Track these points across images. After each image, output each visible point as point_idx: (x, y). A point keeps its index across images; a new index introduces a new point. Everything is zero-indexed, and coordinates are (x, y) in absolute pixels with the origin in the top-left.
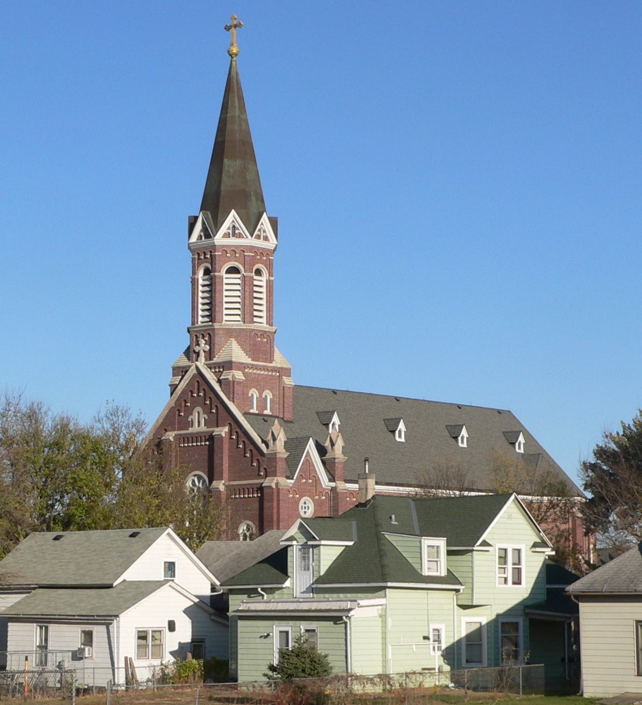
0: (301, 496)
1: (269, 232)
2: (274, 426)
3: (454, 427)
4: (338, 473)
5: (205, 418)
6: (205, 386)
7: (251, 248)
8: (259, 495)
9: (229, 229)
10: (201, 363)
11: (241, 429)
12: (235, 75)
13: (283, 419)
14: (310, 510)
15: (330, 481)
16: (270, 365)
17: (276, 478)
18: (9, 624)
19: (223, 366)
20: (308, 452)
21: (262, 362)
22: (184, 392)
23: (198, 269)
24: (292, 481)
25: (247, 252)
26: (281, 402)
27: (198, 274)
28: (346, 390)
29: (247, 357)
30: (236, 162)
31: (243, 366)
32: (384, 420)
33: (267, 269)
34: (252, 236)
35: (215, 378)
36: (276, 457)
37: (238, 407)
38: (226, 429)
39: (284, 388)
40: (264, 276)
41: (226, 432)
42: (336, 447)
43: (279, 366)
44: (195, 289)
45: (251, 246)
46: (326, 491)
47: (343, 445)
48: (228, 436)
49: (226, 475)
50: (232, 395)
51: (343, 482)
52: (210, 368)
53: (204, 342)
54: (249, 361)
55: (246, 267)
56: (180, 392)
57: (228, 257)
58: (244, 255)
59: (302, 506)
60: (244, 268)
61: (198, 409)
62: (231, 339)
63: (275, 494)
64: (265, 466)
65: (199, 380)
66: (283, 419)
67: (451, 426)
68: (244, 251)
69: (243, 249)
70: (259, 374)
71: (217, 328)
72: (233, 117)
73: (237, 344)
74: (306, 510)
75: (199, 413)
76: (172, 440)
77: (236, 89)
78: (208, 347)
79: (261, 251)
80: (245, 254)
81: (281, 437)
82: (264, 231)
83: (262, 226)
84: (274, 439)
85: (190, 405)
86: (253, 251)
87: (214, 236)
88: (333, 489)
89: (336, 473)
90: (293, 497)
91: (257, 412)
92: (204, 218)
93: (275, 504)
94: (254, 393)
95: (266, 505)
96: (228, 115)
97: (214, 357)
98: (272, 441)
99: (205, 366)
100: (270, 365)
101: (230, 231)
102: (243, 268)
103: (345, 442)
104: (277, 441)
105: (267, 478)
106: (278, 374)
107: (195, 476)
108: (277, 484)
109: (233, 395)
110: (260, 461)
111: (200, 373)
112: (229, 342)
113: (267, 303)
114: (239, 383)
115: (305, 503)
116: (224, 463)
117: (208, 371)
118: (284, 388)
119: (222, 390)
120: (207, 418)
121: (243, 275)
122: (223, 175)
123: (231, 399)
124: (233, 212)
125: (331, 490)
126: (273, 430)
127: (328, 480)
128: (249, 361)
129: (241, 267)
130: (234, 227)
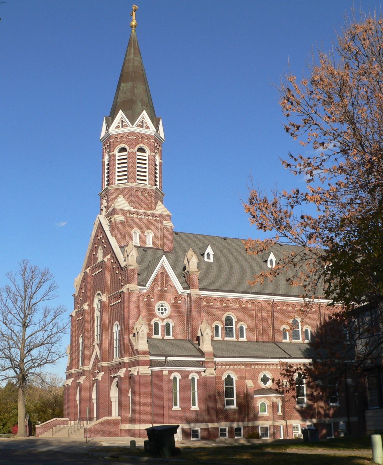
0: (156, 301)
7: (133, 133)
9: (119, 123)
12: (133, 36)
13: (163, 250)
14: (167, 312)
15: (184, 288)
16: (152, 212)
18: (130, 445)
20: (162, 266)
21: (144, 210)
25: (131, 136)
28: (237, 238)
29: (130, 206)
31: (125, 212)
33: (149, 148)
34: (133, 124)
37: (118, 240)
43: (159, 213)
45: (133, 132)
47: (197, 262)
51: (198, 290)
54: (131, 209)
57: (119, 142)
69: (128, 135)
72: (129, 60)
73: (124, 198)
74: (161, 308)
82: (146, 123)
83: (143, 120)
88: (189, 295)
89: (191, 282)
90: (149, 301)
91: (139, 245)
100: (152, 212)
106: (158, 219)
108: (128, 289)
122: (120, 93)
124: (121, 112)
127: (182, 288)
128: (131, 209)
129: (127, 147)
130: (123, 122)
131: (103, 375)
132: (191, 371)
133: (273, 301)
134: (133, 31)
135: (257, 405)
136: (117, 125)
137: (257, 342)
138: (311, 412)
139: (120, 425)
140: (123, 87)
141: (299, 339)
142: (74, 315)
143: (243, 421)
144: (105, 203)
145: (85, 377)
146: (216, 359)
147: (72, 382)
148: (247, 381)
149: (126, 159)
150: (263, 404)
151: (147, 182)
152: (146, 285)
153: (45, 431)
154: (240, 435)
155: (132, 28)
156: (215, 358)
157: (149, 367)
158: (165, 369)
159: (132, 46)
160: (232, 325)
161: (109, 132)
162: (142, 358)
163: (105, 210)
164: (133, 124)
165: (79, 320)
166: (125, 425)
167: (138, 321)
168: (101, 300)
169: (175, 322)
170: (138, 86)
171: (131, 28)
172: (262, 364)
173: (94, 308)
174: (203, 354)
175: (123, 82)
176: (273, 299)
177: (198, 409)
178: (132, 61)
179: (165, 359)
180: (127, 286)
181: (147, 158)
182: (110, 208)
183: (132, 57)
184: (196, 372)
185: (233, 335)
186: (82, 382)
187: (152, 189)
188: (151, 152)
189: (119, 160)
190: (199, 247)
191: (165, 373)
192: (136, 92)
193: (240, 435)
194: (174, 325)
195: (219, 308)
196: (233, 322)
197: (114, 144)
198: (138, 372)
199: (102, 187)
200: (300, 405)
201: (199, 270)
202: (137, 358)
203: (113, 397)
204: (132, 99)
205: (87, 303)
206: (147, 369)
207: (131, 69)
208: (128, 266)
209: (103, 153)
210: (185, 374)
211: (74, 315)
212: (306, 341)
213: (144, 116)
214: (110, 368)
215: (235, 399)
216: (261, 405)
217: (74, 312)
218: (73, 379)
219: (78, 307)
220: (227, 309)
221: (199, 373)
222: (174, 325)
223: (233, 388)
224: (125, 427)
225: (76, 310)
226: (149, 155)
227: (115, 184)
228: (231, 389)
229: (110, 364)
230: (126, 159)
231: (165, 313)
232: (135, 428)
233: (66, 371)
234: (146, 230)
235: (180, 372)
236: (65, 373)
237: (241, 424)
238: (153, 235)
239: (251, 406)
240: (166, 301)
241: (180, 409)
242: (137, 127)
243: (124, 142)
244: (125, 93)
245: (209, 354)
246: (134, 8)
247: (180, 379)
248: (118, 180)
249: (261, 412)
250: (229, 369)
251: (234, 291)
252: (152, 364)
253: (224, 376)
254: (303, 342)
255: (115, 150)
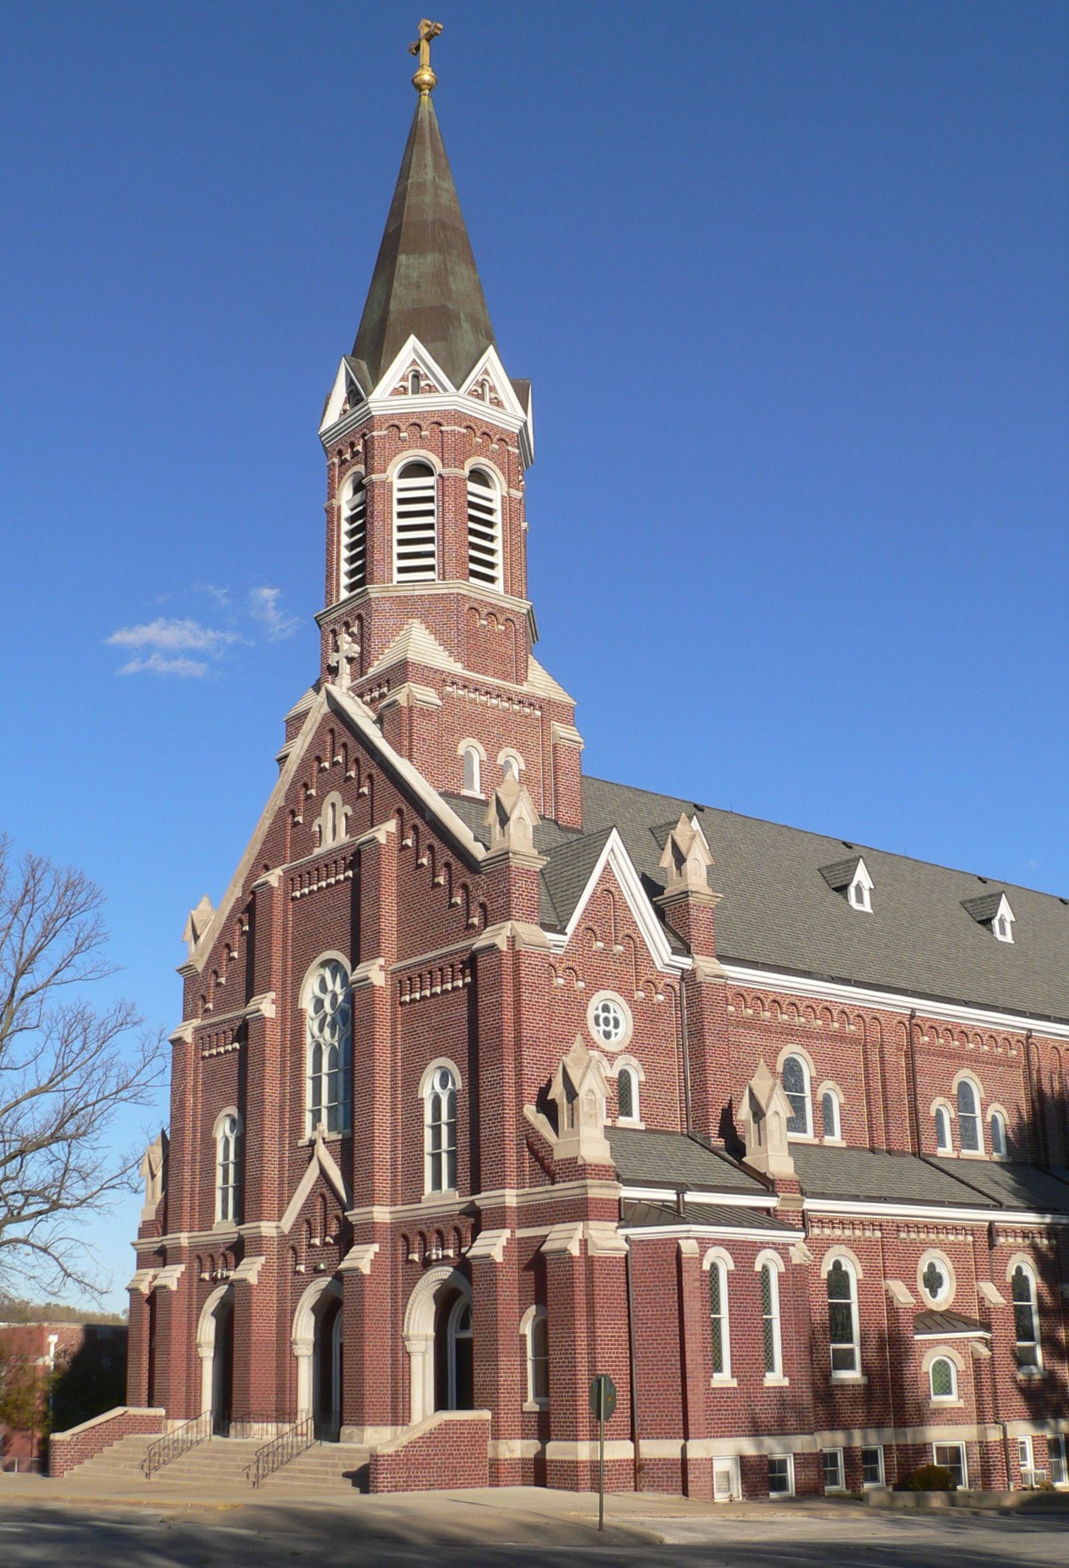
1: (504, 390)
2: (504, 786)
3: (979, 902)
4: (698, 934)
5: (346, 815)
6: (346, 737)
7: (457, 417)
8: (468, 980)
9: (404, 378)
10: (341, 687)
11: (423, 817)
13: (556, 822)
14: (621, 1030)
15: (675, 951)
16: (518, 688)
17: (509, 924)
19: (388, 681)
20: (607, 868)
21: (493, 676)
22: (303, 766)
23: (339, 482)
24: (566, 938)
25: (449, 424)
26: (550, 781)
27: (339, 495)
29: (452, 659)
30: (426, 258)
32: (819, 870)
34: (458, 387)
35: (371, 714)
36: (509, 867)
37: (424, 771)
38: (391, 826)
39: (555, 746)
40: (495, 489)
41: (388, 834)
42: (689, 865)
44: (332, 530)
45: (457, 411)
46: (668, 981)
47: (709, 863)
48: (394, 846)
49: (390, 939)
50: (406, 743)
52: (361, 696)
53: (349, 639)
54: (457, 668)
55: (446, 456)
56: (294, 769)
58: (441, 432)
59: (597, 1018)
60: (443, 460)
61: (335, 796)
62: (410, 621)
63: (507, 969)
64: (482, 899)
65: (334, 726)
66: (556, 822)
67: (971, 901)
68: (440, 424)
70: (484, 705)
71: (376, 598)
72: (421, 185)
73: (427, 632)
74: (603, 1015)
75: (333, 805)
76: (276, 885)
77: (428, 137)
78: (357, 648)
79: (485, 429)
80: (442, 428)
81: (525, 816)
82: (492, 389)
84: (504, 819)
85: (317, 794)
86: (465, 424)
87: (368, 394)
88: (688, 977)
90: (568, 987)
92: (349, 369)
93: (508, 998)
94: (471, 748)
95: (484, 1000)
96: (410, 181)
97: (370, 665)
98: (498, 827)
99: (350, 693)
100: (518, 688)
101: (409, 385)
102: (439, 460)
103: (712, 851)
104: (511, 823)
105: (488, 929)
106: (538, 713)
107: (324, 964)
108: (512, 940)
109: (411, 742)
110: (471, 888)
111: (337, 711)
112: (406, 627)
113: (504, 547)
114: (426, 714)
115: (606, 1009)
116: (383, 912)
117: (356, 701)
118: (555, 746)
119: (384, 737)
120: (350, 813)
121: (440, 475)
122: (396, 284)
123: (405, 751)
124: (412, 339)
125: (682, 979)
126: (499, 794)
127: (670, 950)
128: (457, 668)
129: (434, 460)
131: (376, 1253)
132: (761, 1243)
133: (912, 1017)
134: (425, 99)
135: (924, 1369)
136: (396, 384)
137: (889, 1152)
138: (1054, 1398)
139: (490, 1442)
140: (408, 267)
141: (976, 1148)
142: (189, 1038)
143: (879, 1425)
144: (349, 646)
145: (262, 1259)
146: (810, 1204)
147: (178, 1279)
148: (889, 1282)
149: (430, 499)
150: (942, 1368)
151: (499, 587)
152: (565, 928)
153: (86, 1456)
154: (873, 1477)
155: (421, 90)
156: (807, 1200)
157: (616, 1224)
158: (685, 1235)
159: (428, 145)
160: (802, 1091)
161: (370, 405)
162: (598, 1191)
163: (348, 671)
164: (458, 387)
165: (211, 1056)
166: (510, 1442)
167: (571, 1054)
168: (367, 979)
169: (648, 1068)
170: (457, 268)
171: (416, 92)
172: (927, 1228)
173: (299, 1015)
174: (767, 1185)
175: (407, 253)
176: (913, 1010)
177: (786, 1382)
178: (430, 188)
179: (674, 1198)
180: (507, 928)
181: (496, 505)
182: (376, 663)
183: (430, 176)
184: (775, 1246)
185: (805, 1124)
186: (253, 1279)
187: (517, 609)
188: (509, 487)
189: (402, 501)
190: (649, 823)
191: (689, 1248)
192: (453, 287)
193: (873, 1477)
194: (644, 1080)
195: (766, 1029)
196: (802, 1080)
197: (387, 445)
198: (584, 1243)
199: (328, 592)
200: (1025, 1369)
201: (714, 891)
202: (578, 1191)
203: (418, 1337)
204: (445, 306)
205: (272, 995)
206: (612, 1234)
207: (431, 213)
208: (511, 855)
209: (331, 478)
210: (743, 1252)
211: (189, 1038)
212: (996, 1156)
213: (487, 364)
214: (405, 1230)
215: (855, 1345)
216: (934, 1369)
217: (190, 1030)
218: (182, 1268)
219: (206, 1010)
220: (790, 1033)
221: (783, 1249)
222: (644, 1080)
223: (848, 1306)
224: (512, 1451)
225: (196, 1022)
226: (503, 497)
227: (392, 581)
228: (845, 1311)
229: (409, 1214)
230: (430, 499)
231: (616, 1034)
232: (576, 1454)
233: (135, 1239)
234: (500, 748)
235: (728, 1245)
236: (133, 1244)
237: (873, 1435)
238: (523, 768)
239: (909, 1371)
240: (619, 990)
241: (734, 1383)
242: (470, 398)
243: (423, 443)
244: (418, 285)
245: (789, 1185)
246: (426, 30)
247: (729, 1273)
248: (402, 570)
249: (936, 1394)
250: (839, 1241)
251: (809, 972)
252: (625, 1214)
253: (827, 1267)
254: (955, 1157)
255: (390, 468)
